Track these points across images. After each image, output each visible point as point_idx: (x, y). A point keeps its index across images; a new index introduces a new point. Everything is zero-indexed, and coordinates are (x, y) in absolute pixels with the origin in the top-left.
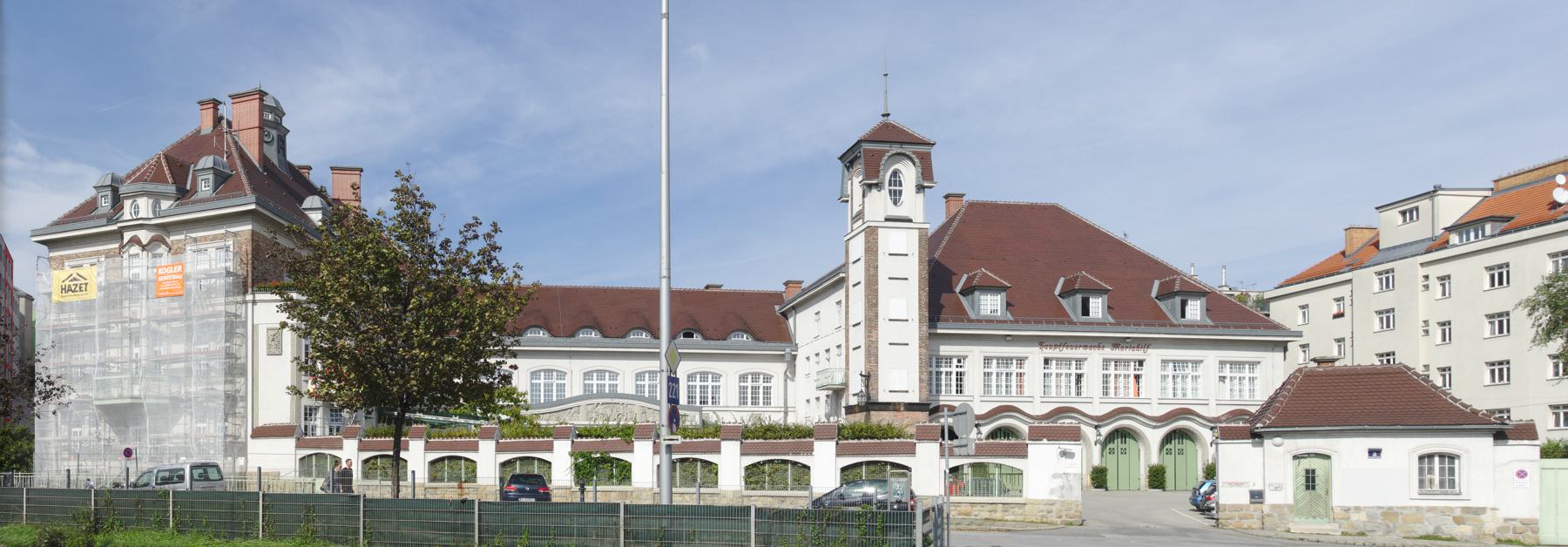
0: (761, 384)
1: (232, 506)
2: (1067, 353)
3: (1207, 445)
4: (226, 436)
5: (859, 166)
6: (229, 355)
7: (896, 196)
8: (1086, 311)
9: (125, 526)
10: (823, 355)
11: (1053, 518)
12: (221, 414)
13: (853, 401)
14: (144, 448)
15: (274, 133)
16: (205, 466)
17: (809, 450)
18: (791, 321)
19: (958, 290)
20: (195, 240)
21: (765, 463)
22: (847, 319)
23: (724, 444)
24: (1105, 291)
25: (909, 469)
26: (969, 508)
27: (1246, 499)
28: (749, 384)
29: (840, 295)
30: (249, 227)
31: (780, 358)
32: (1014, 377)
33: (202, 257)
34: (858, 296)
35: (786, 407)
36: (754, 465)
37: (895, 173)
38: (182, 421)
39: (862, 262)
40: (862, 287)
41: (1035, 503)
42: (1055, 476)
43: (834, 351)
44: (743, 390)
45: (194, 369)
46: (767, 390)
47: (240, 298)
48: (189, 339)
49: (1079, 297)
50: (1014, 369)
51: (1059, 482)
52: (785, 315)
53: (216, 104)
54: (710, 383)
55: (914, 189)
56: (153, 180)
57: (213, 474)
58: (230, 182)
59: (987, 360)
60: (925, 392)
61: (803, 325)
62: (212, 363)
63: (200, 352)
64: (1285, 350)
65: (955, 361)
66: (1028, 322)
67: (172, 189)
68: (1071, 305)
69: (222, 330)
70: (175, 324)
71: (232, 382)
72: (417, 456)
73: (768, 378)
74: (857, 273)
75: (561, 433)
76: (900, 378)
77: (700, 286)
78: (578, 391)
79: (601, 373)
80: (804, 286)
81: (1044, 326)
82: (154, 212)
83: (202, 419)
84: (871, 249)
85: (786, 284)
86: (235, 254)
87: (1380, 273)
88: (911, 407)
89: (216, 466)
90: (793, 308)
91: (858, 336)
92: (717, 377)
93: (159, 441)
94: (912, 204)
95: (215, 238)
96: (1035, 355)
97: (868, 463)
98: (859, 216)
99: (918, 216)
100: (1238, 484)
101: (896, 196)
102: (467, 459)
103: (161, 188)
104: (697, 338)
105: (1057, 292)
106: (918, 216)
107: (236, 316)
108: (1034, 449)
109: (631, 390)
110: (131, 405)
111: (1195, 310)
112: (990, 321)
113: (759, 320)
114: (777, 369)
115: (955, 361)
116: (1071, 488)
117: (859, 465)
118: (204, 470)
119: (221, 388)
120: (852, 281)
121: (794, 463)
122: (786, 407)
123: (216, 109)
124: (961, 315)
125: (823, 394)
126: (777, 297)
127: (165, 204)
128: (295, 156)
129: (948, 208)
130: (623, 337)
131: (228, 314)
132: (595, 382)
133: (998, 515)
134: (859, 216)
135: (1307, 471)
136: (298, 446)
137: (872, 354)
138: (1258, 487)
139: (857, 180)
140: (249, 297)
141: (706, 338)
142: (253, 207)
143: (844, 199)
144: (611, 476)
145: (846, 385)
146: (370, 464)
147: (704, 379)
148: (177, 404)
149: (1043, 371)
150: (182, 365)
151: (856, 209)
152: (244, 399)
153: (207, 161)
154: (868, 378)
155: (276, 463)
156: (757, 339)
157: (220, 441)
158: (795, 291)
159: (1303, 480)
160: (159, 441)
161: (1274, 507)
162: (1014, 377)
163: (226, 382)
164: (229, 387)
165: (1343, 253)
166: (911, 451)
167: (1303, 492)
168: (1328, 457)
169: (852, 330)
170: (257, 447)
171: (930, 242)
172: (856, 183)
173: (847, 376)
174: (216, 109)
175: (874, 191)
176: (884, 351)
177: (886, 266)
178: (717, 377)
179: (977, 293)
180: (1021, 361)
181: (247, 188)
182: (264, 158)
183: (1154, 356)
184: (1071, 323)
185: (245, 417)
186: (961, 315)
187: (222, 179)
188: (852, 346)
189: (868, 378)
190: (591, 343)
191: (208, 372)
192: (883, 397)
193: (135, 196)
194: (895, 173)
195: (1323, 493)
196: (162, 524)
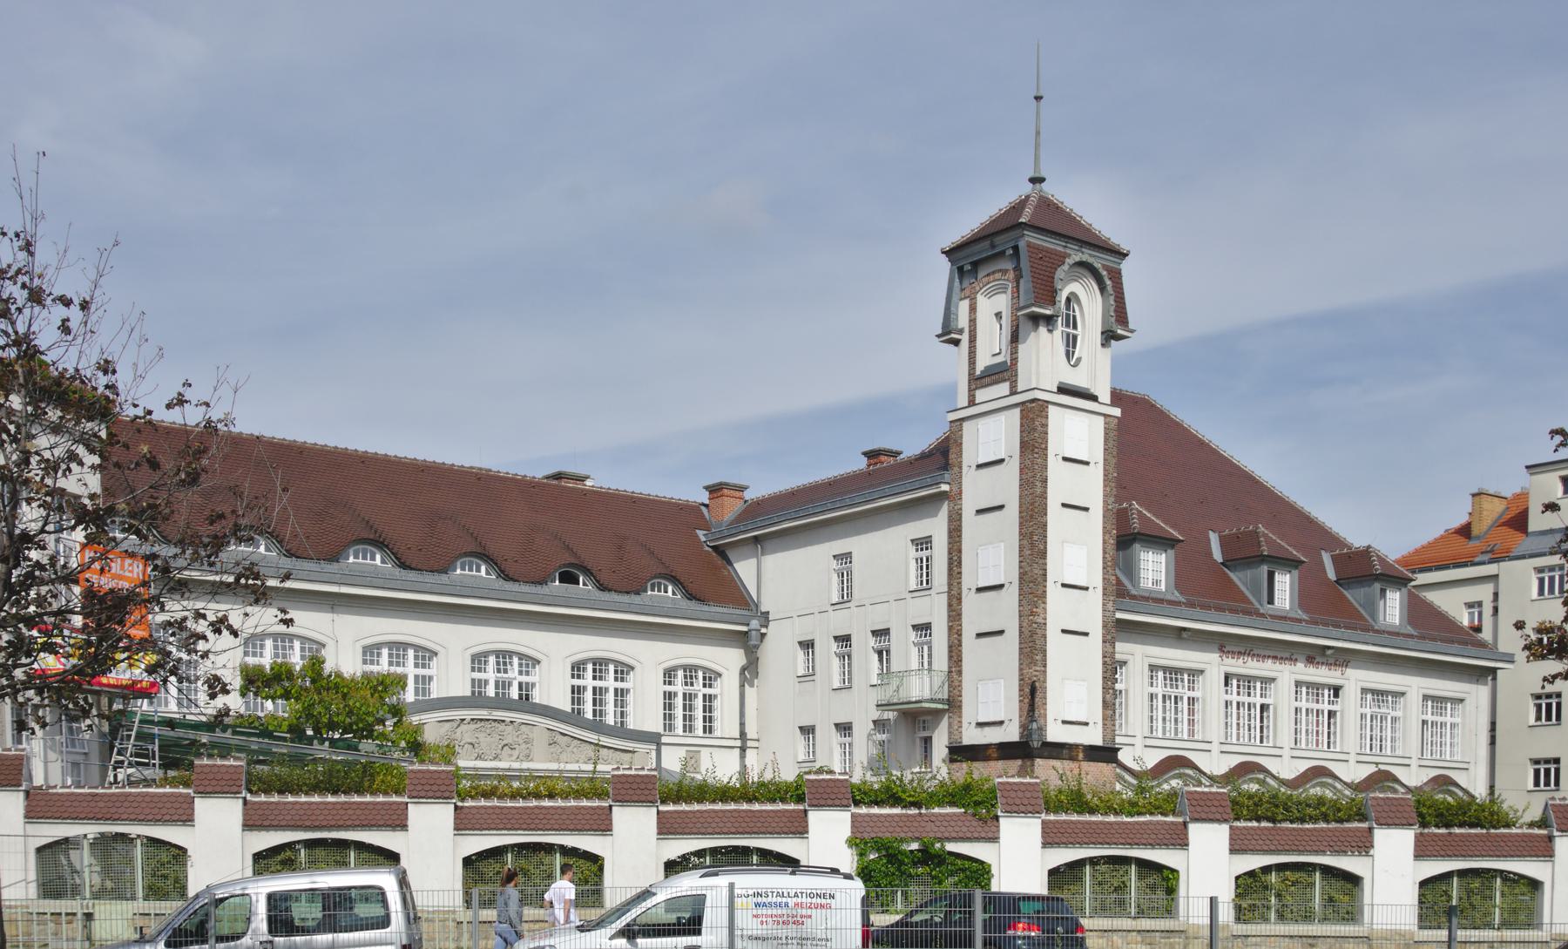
2: (1252, 667)
17: (1364, 846)
21: (1266, 870)
28: (679, 687)
35: (743, 735)
36: (1251, 874)
55: (1098, 338)
64: (1494, 679)
73: (711, 677)
74: (986, 485)
77: (538, 472)
78: (460, 687)
80: (749, 495)
87: (1540, 570)
92: (623, 670)
96: (1213, 664)
98: (1003, 372)
104: (584, 586)
114: (729, 660)
117: (1447, 876)
122: (743, 735)
126: (687, 514)
141: (602, 587)
147: (689, 681)
156: (691, 596)
158: (731, 508)
165: (1465, 531)
172: (992, 308)
178: (623, 670)
179: (1137, 546)
183: (1355, 679)
192: (1056, 733)
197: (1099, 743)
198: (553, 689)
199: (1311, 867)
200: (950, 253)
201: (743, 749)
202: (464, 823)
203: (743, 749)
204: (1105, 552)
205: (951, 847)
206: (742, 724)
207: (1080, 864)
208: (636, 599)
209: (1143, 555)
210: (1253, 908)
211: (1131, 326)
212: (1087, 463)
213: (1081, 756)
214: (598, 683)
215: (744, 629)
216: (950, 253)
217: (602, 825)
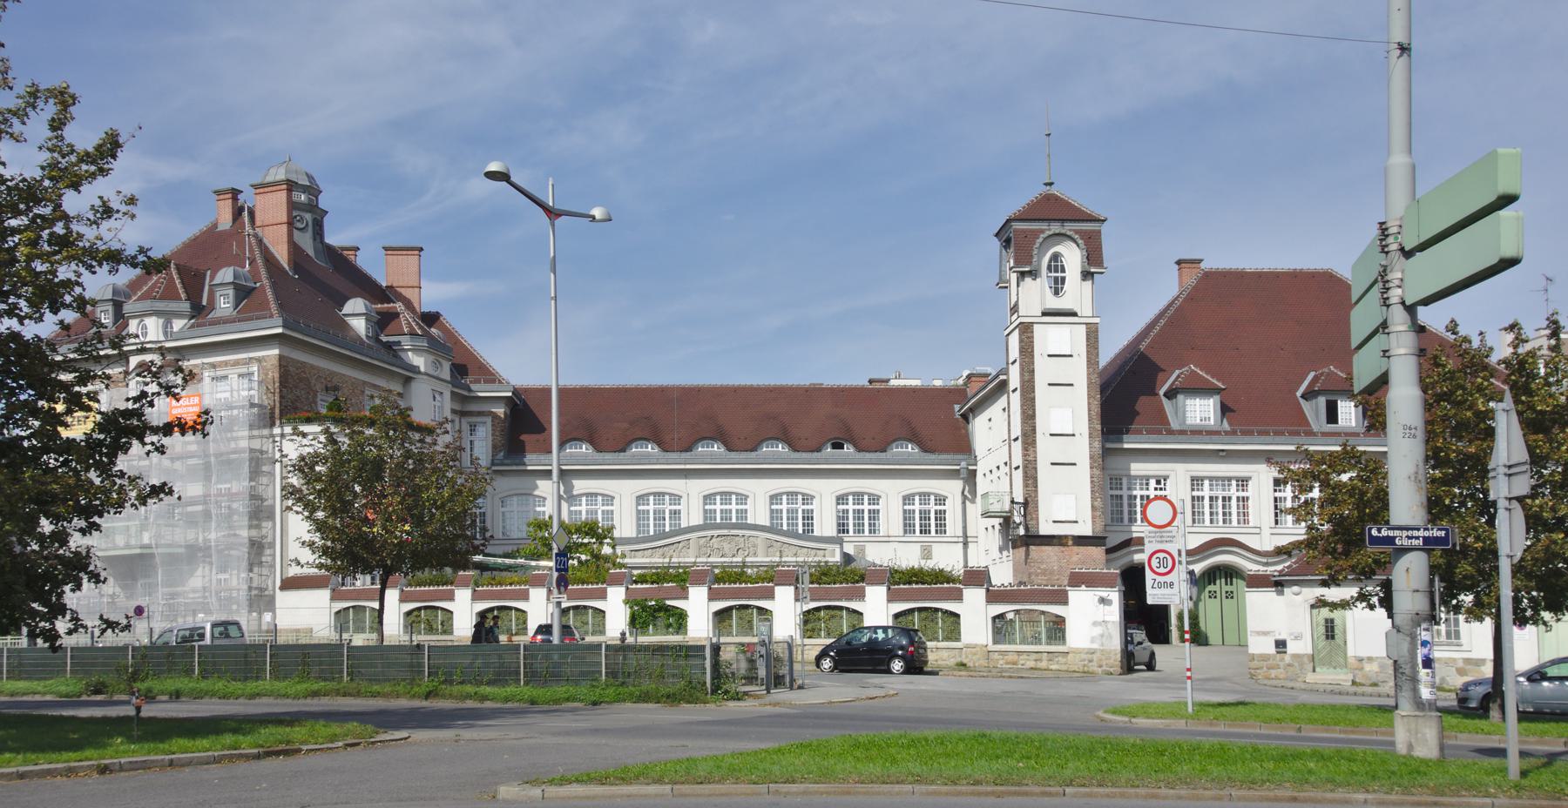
0: (933, 508)
1: (246, 656)
4: (250, 588)
6: (255, 497)
8: (1332, 416)
9: (157, 675)
11: (1094, 667)
12: (245, 564)
14: (156, 603)
15: (308, 217)
16: (225, 624)
19: (1162, 392)
20: (213, 366)
25: (958, 616)
26: (1015, 657)
27: (1272, 650)
30: (276, 352)
31: (954, 474)
32: (1234, 502)
33: (222, 385)
35: (965, 536)
37: (1056, 257)
38: (199, 572)
41: (1077, 651)
42: (1095, 624)
44: (907, 516)
45: (214, 512)
46: (940, 516)
47: (266, 432)
48: (208, 478)
49: (1322, 401)
51: (1098, 630)
52: (965, 417)
53: (235, 193)
54: (866, 507)
55: (1079, 276)
56: (162, 298)
57: (233, 631)
58: (254, 294)
59: (1196, 481)
62: (235, 505)
63: (220, 494)
65: (1153, 483)
66: (1250, 433)
67: (185, 306)
68: (1314, 411)
69: (246, 469)
70: (192, 461)
71: (258, 527)
72: (395, 607)
73: (941, 500)
74: (1014, 380)
75: (698, 577)
76: (1068, 504)
77: (862, 382)
78: (696, 519)
79: (726, 496)
82: (165, 333)
83: (223, 569)
84: (1027, 350)
86: (260, 383)
88: (1081, 541)
89: (237, 624)
92: (874, 499)
93: (173, 596)
94: (1077, 294)
95: (236, 363)
97: (920, 610)
99: (1085, 310)
100: (1265, 634)
101: (1058, 286)
102: (517, 610)
103: (173, 306)
104: (848, 449)
106: (1085, 310)
107: (262, 452)
108: (1074, 595)
109: (764, 520)
110: (141, 555)
112: (1197, 433)
113: (930, 425)
114: (952, 489)
115: (1153, 483)
116: (1110, 637)
117: (911, 611)
118: (224, 627)
119: (244, 533)
120: (1012, 387)
122: (965, 536)
123: (235, 199)
124: (1160, 425)
127: (178, 324)
128: (335, 237)
130: (754, 449)
131: (252, 450)
132: (718, 507)
133: (1043, 665)
134: (1015, 309)
136: (333, 599)
140: (277, 431)
141: (859, 449)
142: (280, 330)
144: (669, 626)
146: (412, 618)
148: (195, 554)
149: (1271, 495)
150: (199, 508)
152: (272, 545)
153: (226, 275)
155: (307, 615)
157: (243, 594)
159: (1322, 630)
160: (173, 596)
161: (1295, 656)
162: (1234, 502)
163: (250, 527)
164: (254, 533)
166: (958, 597)
167: (1322, 643)
170: (285, 599)
174: (235, 199)
175: (1028, 280)
176: (1044, 472)
177: (1044, 371)
178: (874, 499)
179: (1180, 397)
180: (1243, 482)
181: (273, 306)
182: (295, 249)
185: (273, 566)
186: (1160, 425)
187: (243, 293)
190: (713, 458)
191: (230, 516)
192: (1045, 529)
193: (142, 315)
194: (1056, 257)
196: (188, 672)
198: (759, 514)
199: (841, 608)
200: (997, 235)
201: (966, 544)
203: (966, 544)
205: (668, 603)
206: (965, 528)
207: (730, 609)
208: (882, 455)
209: (1189, 402)
210: (813, 630)
216: (997, 235)
217: (958, 597)
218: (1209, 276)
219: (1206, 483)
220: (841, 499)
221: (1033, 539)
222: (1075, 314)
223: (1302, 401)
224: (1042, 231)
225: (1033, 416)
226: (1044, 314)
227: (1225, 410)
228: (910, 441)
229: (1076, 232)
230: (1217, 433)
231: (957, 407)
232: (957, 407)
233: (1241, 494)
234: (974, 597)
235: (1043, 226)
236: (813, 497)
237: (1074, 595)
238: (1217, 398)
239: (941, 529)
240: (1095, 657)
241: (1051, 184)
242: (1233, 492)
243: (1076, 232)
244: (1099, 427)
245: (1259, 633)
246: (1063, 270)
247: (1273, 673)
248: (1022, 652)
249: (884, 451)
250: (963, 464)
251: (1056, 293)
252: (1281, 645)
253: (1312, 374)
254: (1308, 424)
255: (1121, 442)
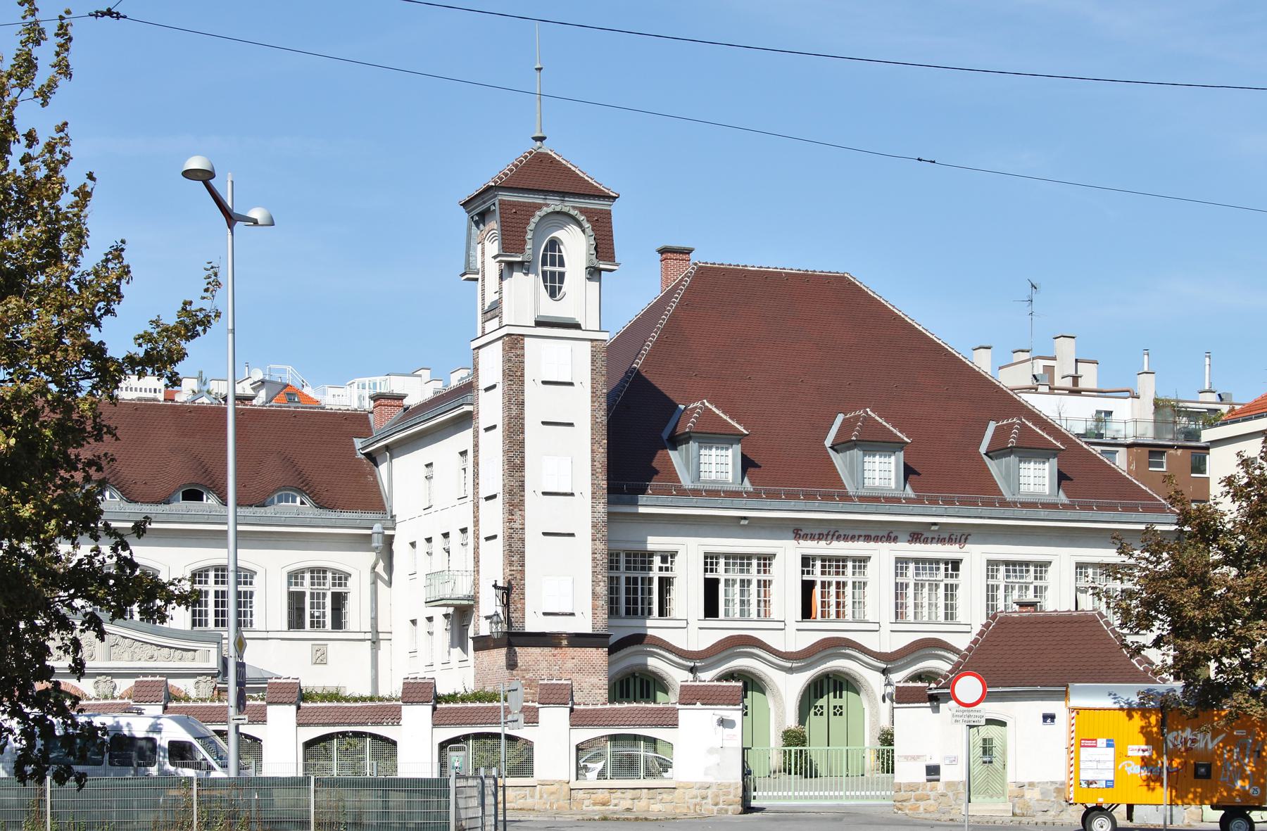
3: (872, 706)
5: (493, 225)
7: (554, 285)
10: (438, 541)
13: (485, 629)
18: (383, 469)
22: (476, 485)
23: (271, 710)
24: (900, 445)
25: (394, 743)
27: (922, 777)
29: (463, 439)
31: (362, 542)
34: (493, 447)
35: (375, 642)
37: (554, 244)
39: (498, 391)
40: (498, 433)
41: (688, 786)
42: (711, 751)
43: (456, 536)
44: (296, 601)
50: (754, 575)
52: (372, 458)
55: (583, 273)
60: (603, 615)
61: (402, 478)
74: (490, 408)
81: (801, 504)
84: (514, 373)
85: (376, 398)
88: (579, 640)
90: (387, 448)
91: (493, 517)
94: (579, 297)
96: (788, 553)
97: (477, 736)
101: (554, 285)
105: (828, 442)
106: (590, 321)
108: (408, 711)
111: (1036, 478)
112: (714, 493)
114: (358, 564)
120: (483, 422)
121: (374, 737)
125: (438, 613)
129: (665, 269)
134: (493, 311)
135: (985, 740)
137: (515, 552)
138: (933, 762)
139: (493, 248)
143: (471, 274)
145: (474, 598)
151: (491, 298)
154: (509, 592)
161: (950, 784)
167: (977, 768)
168: (1003, 724)
169: (482, 503)
171: (610, 355)
173: (476, 584)
175: (518, 275)
176: (534, 545)
177: (538, 403)
184: (845, 497)
188: (483, 534)
189: (509, 592)
192: (534, 624)
195: (999, 767)
197: (589, 631)
200: (465, 205)
201: (375, 642)
202: (439, 720)
204: (593, 460)
206: (375, 619)
208: (260, 511)
211: (617, 261)
212: (571, 384)
213: (565, 642)
214: (220, 588)
215: (369, 532)
216: (465, 205)
218: (705, 274)
219: (722, 561)
220: (295, 576)
221: (514, 639)
222: (577, 326)
223: (831, 452)
224: (539, 207)
225: (521, 467)
226: (539, 324)
227: (747, 464)
228: (301, 491)
229: (583, 211)
230: (897, 500)
231: (358, 443)
232: (358, 443)
233: (763, 577)
234: (417, 717)
235: (538, 200)
236: (348, 576)
237: (408, 711)
238: (738, 448)
239: (338, 623)
240: (709, 792)
241: (541, 139)
242: (754, 575)
243: (583, 211)
244: (604, 484)
245: (906, 758)
246: (562, 264)
247: (922, 804)
248: (628, 795)
249: (168, 502)
250: (377, 527)
251: (553, 294)
252: (933, 771)
253: (840, 418)
254: (838, 481)
255: (636, 504)
